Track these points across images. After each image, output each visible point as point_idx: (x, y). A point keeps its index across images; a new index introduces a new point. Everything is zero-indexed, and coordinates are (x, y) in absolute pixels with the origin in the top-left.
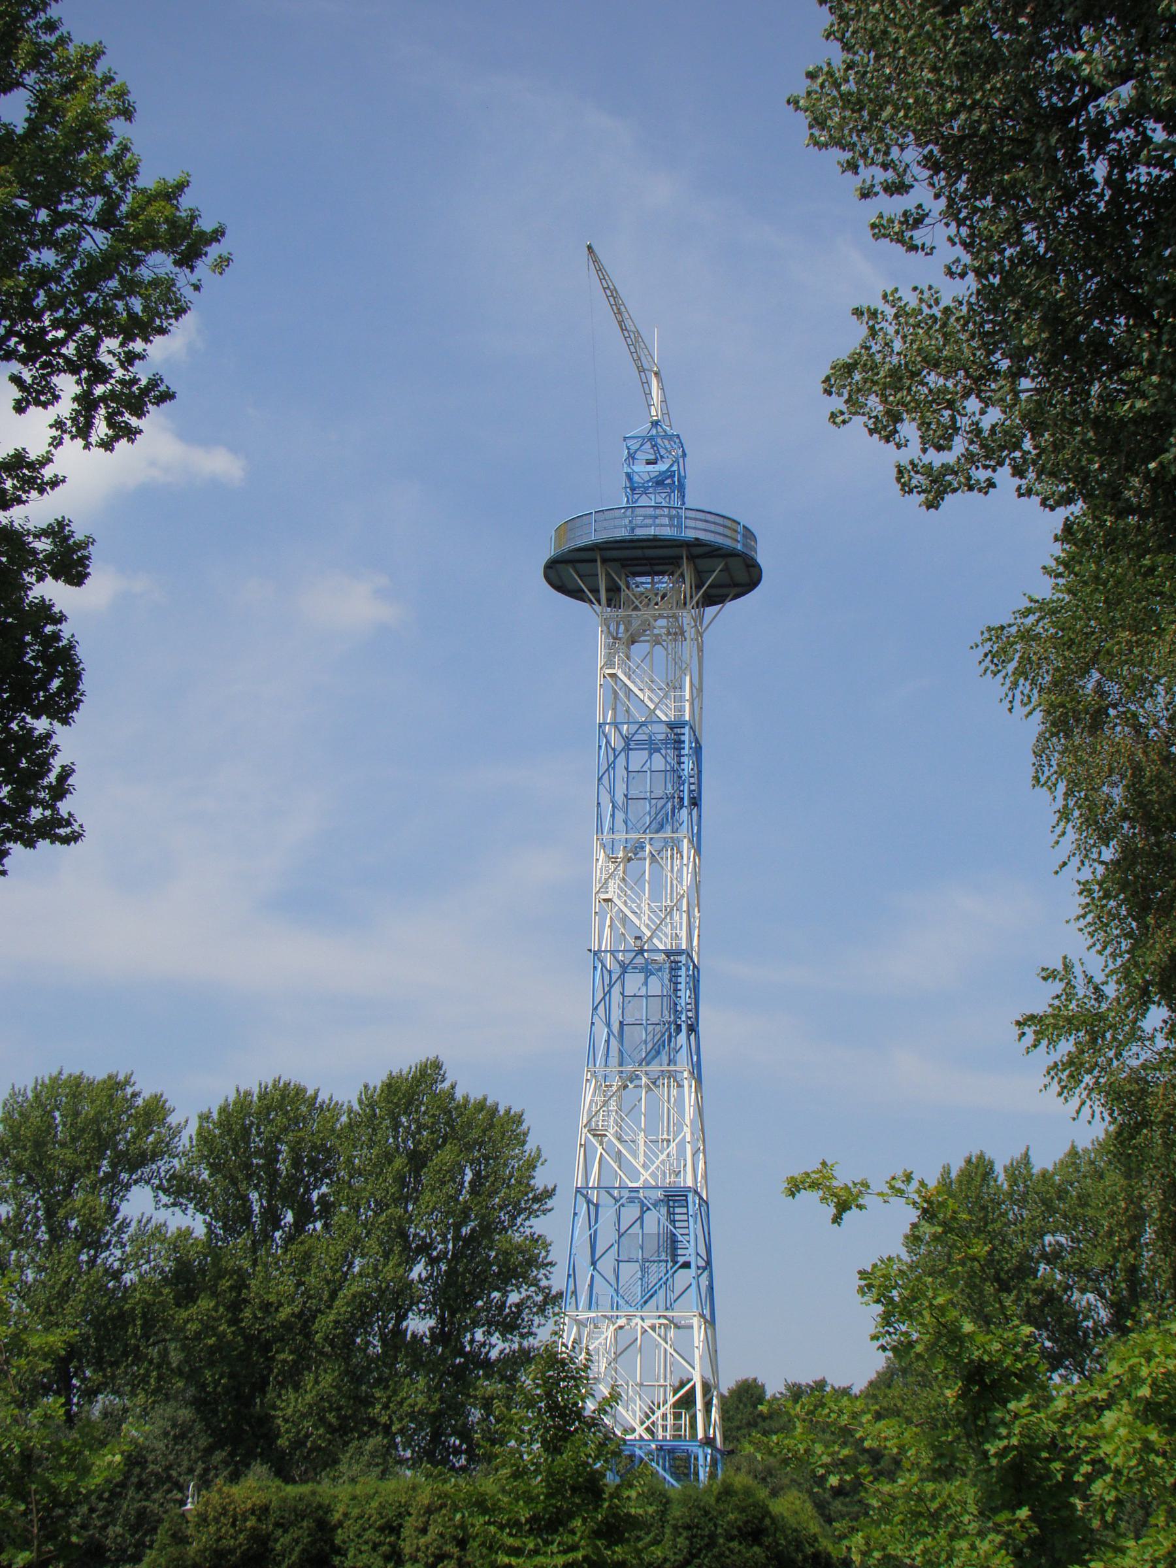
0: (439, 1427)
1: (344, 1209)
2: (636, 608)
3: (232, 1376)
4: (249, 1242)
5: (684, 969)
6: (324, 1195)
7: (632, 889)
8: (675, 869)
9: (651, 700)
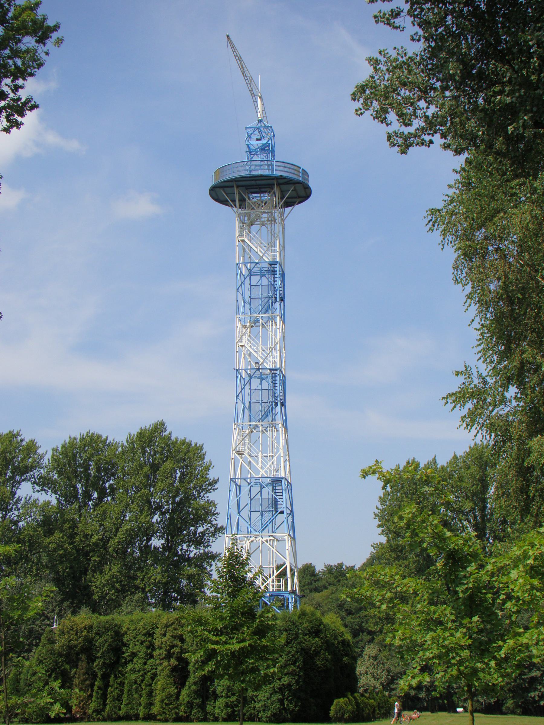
0: (168, 588)
1: (121, 491)
2: (253, 209)
3: (71, 568)
4: (77, 506)
5: (278, 377)
6: (112, 485)
7: (253, 340)
8: (274, 330)
9: (261, 252)
